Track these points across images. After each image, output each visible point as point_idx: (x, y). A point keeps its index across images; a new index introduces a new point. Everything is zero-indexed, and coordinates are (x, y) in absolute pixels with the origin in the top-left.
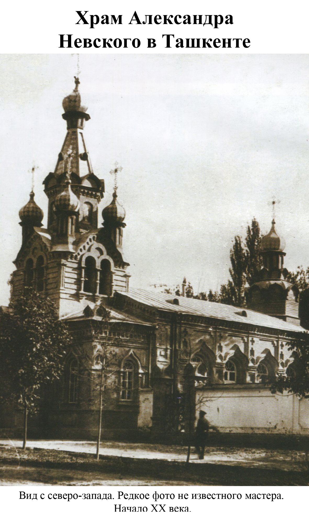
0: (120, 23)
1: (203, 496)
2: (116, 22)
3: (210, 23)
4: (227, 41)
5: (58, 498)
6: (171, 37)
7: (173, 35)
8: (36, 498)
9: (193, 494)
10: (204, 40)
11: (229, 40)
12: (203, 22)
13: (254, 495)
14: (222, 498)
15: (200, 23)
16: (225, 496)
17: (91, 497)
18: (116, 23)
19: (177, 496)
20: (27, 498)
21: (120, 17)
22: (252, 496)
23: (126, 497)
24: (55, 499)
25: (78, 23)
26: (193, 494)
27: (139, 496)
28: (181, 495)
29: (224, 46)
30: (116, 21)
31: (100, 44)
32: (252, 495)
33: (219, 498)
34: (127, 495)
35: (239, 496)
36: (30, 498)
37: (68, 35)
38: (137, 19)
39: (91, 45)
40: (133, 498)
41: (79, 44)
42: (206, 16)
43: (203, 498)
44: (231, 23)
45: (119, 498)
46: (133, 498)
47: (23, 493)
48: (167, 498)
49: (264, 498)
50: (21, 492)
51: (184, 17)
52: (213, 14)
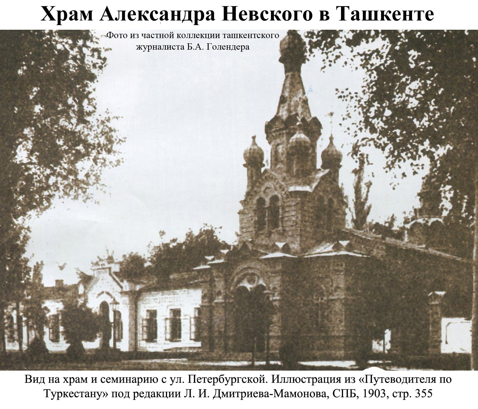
0: (90, 19)
2: (85, 18)
3: (190, 19)
4: (408, 13)
6: (346, 9)
7: (348, 7)
10: (382, 12)
11: (411, 12)
15: (179, 19)
17: (323, 381)
18: (85, 19)
21: (90, 12)
25: (43, 20)
29: (405, 19)
30: (85, 17)
31: (268, 16)
39: (257, 18)
41: (244, 17)
44: (213, 19)
50: (26, 376)
51: (161, 13)
52: (193, 9)
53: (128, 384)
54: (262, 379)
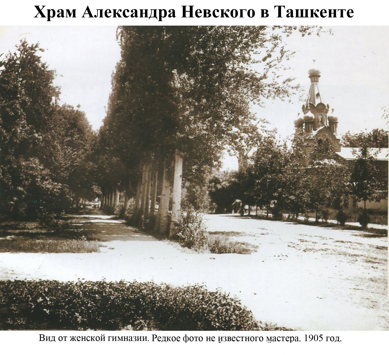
0: (74, 16)
1: (228, 339)
2: (70, 15)
3: (155, 16)
4: (332, 12)
5: (81, 340)
6: (282, 8)
7: (284, 6)
8: (54, 340)
9: (219, 337)
10: (312, 11)
11: (335, 11)
12: (149, 15)
13: (274, 338)
14: (246, 341)
15: (146, 16)
16: (248, 339)
18: (70, 16)
19: (205, 339)
20: (47, 340)
21: (74, 11)
22: (272, 339)
23: (159, 339)
24: (79, 341)
25: (36, 17)
26: (219, 337)
27: (171, 339)
28: (208, 338)
29: (330, 16)
30: (70, 15)
31: (219, 14)
32: (272, 338)
33: (242, 341)
34: (161, 338)
35: (261, 339)
36: (49, 340)
37: (183, 6)
38: (90, 13)
39: (210, 15)
40: (165, 341)
41: (199, 15)
42: (151, 10)
43: (228, 341)
44: (174, 16)
45: (153, 341)
46: (165, 341)
47: (42, 336)
48: (196, 341)
49: (283, 341)
50: (40, 335)
51: (132, 11)
52: (158, 8)
53: (126, 342)
54: (103, 337)
